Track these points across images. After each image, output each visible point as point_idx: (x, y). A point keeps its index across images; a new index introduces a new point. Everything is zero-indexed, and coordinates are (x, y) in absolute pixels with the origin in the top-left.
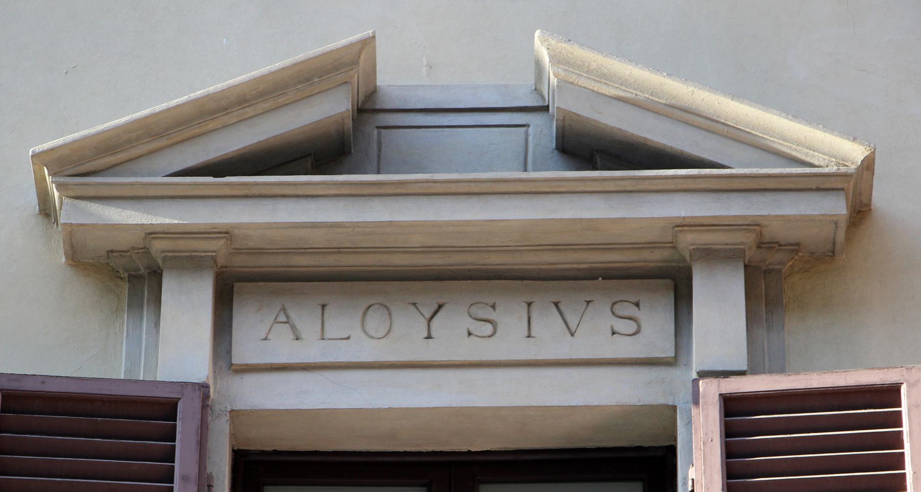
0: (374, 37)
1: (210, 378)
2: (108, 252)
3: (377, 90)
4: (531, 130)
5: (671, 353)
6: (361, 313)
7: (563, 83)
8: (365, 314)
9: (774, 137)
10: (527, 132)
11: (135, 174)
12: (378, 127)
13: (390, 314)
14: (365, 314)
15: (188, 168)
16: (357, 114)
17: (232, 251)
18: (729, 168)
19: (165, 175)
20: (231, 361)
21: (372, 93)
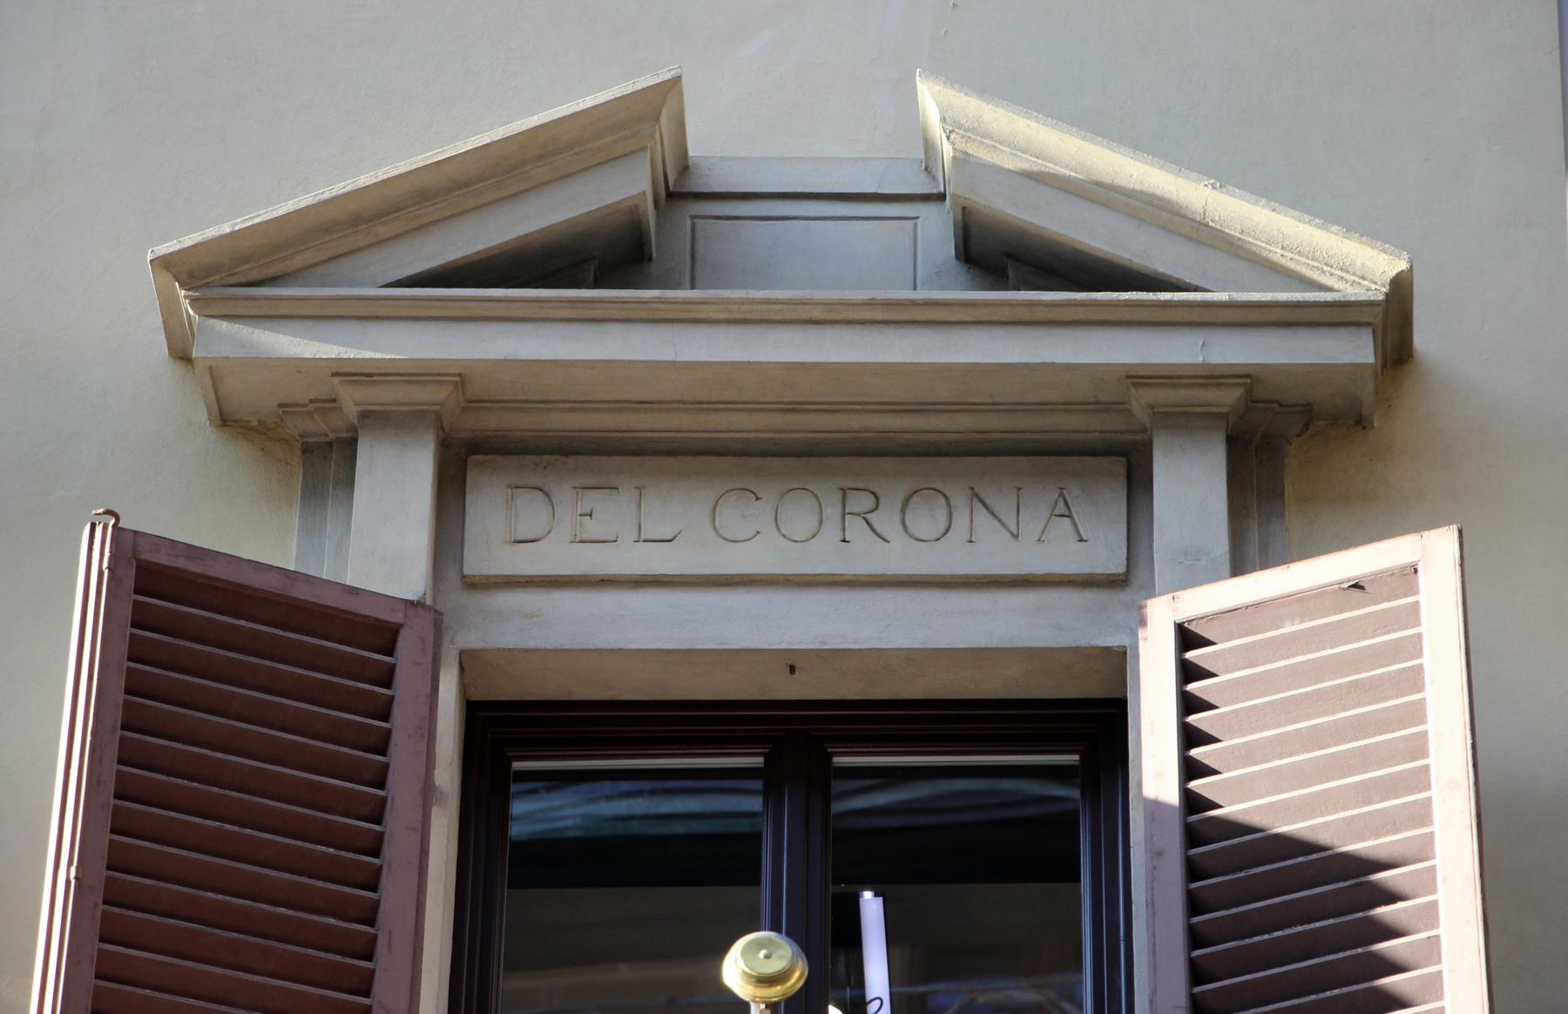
0: (677, 80)
1: (427, 596)
2: (280, 406)
3: (690, 162)
4: (919, 222)
5: (1120, 568)
6: (899, 506)
7: (962, 160)
8: (903, 511)
9: (1260, 240)
10: (915, 226)
11: (315, 284)
12: (693, 217)
13: (547, 495)
14: (903, 511)
15: (420, 273)
16: (666, 200)
17: (465, 404)
18: (1197, 289)
19: (380, 285)
20: (462, 573)
21: (685, 168)
